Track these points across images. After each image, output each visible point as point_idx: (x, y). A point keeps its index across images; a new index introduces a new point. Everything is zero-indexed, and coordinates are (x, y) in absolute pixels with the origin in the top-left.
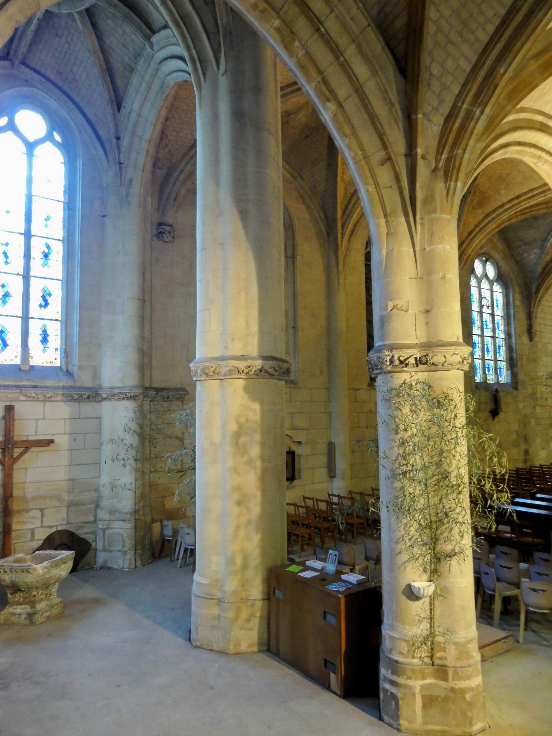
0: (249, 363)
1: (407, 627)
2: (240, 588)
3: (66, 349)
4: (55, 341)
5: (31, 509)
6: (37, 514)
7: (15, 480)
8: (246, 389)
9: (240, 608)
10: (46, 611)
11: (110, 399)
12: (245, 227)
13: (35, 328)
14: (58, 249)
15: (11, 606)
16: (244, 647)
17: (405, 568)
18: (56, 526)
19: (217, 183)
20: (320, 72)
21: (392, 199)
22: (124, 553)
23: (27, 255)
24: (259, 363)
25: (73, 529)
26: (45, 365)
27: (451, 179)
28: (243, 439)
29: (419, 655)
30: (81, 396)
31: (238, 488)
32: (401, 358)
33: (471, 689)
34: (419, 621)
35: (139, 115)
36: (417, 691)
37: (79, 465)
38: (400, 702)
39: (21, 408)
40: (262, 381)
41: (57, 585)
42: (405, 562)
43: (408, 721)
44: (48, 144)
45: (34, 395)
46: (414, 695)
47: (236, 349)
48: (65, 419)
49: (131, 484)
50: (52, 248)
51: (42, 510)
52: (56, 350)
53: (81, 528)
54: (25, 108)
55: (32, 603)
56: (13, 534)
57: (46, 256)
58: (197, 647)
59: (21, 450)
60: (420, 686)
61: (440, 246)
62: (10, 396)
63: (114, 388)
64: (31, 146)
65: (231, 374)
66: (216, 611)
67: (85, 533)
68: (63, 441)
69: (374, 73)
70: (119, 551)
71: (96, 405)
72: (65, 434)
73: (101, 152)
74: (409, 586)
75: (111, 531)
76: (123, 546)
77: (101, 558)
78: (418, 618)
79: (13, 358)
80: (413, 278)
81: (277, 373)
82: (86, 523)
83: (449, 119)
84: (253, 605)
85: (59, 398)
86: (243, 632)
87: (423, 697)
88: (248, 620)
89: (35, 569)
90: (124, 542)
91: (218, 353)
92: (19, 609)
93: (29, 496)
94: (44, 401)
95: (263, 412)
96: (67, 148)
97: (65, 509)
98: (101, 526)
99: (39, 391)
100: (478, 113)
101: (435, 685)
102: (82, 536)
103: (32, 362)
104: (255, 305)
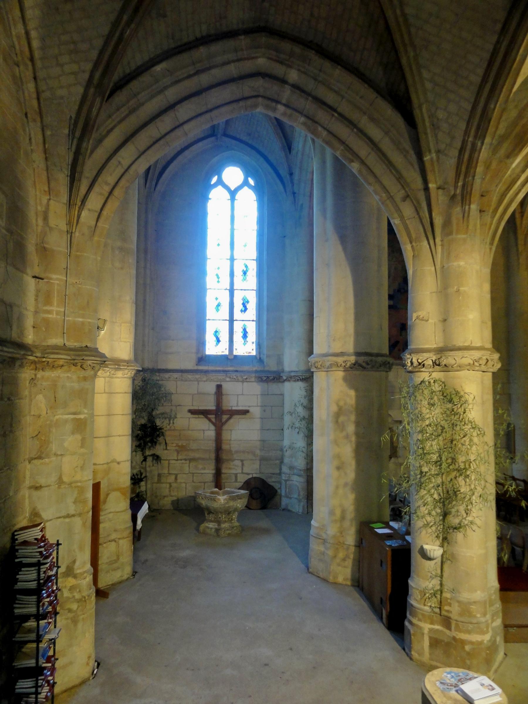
0: (345, 358)
1: (421, 580)
2: (338, 534)
3: (259, 342)
4: (252, 337)
6: (238, 463)
8: (345, 379)
9: (337, 549)
10: (228, 530)
11: (289, 381)
12: (345, 249)
13: (238, 327)
14: (253, 267)
15: (207, 522)
16: (340, 579)
17: (421, 532)
18: (252, 474)
19: (325, 218)
20: (343, 143)
21: (414, 226)
22: (300, 501)
23: (232, 274)
24: (353, 359)
26: (245, 354)
27: (465, 203)
28: (341, 419)
29: (429, 604)
30: (268, 377)
31: (338, 456)
32: (419, 361)
33: (472, 643)
34: (431, 577)
35: (303, 154)
36: (426, 631)
37: (268, 430)
38: (412, 637)
39: (227, 387)
40: (358, 373)
42: (421, 528)
43: (418, 654)
44: (246, 188)
45: (234, 377)
46: (423, 634)
47: (337, 348)
48: (257, 395)
49: (304, 447)
50: (249, 267)
51: (242, 461)
52: (253, 343)
53: (271, 477)
54: (228, 166)
55: (219, 523)
56: (223, 476)
57: (245, 273)
58: (310, 573)
59: (228, 416)
60: (429, 629)
61: (455, 264)
62: (220, 378)
63: (292, 372)
64: (233, 194)
65: (331, 368)
66: (322, 548)
68: (256, 411)
69: (387, 133)
70: (296, 498)
71: (280, 385)
72: (258, 406)
73: (281, 187)
74: (422, 547)
75: (291, 482)
76: (299, 495)
77: (284, 502)
78: (430, 574)
79: (224, 350)
80: (434, 292)
81: (369, 367)
82: (273, 474)
83: (462, 150)
84: (348, 549)
85: (253, 379)
86: (340, 568)
87: (430, 638)
88: (344, 560)
89: (219, 499)
90: (299, 493)
91: (324, 351)
92: (211, 525)
93: (233, 450)
94: (243, 382)
95: (357, 397)
96: (258, 189)
98: (284, 478)
99: (238, 374)
100: (479, 144)
101: (442, 631)
102: (270, 484)
103: (235, 353)
104: (352, 311)
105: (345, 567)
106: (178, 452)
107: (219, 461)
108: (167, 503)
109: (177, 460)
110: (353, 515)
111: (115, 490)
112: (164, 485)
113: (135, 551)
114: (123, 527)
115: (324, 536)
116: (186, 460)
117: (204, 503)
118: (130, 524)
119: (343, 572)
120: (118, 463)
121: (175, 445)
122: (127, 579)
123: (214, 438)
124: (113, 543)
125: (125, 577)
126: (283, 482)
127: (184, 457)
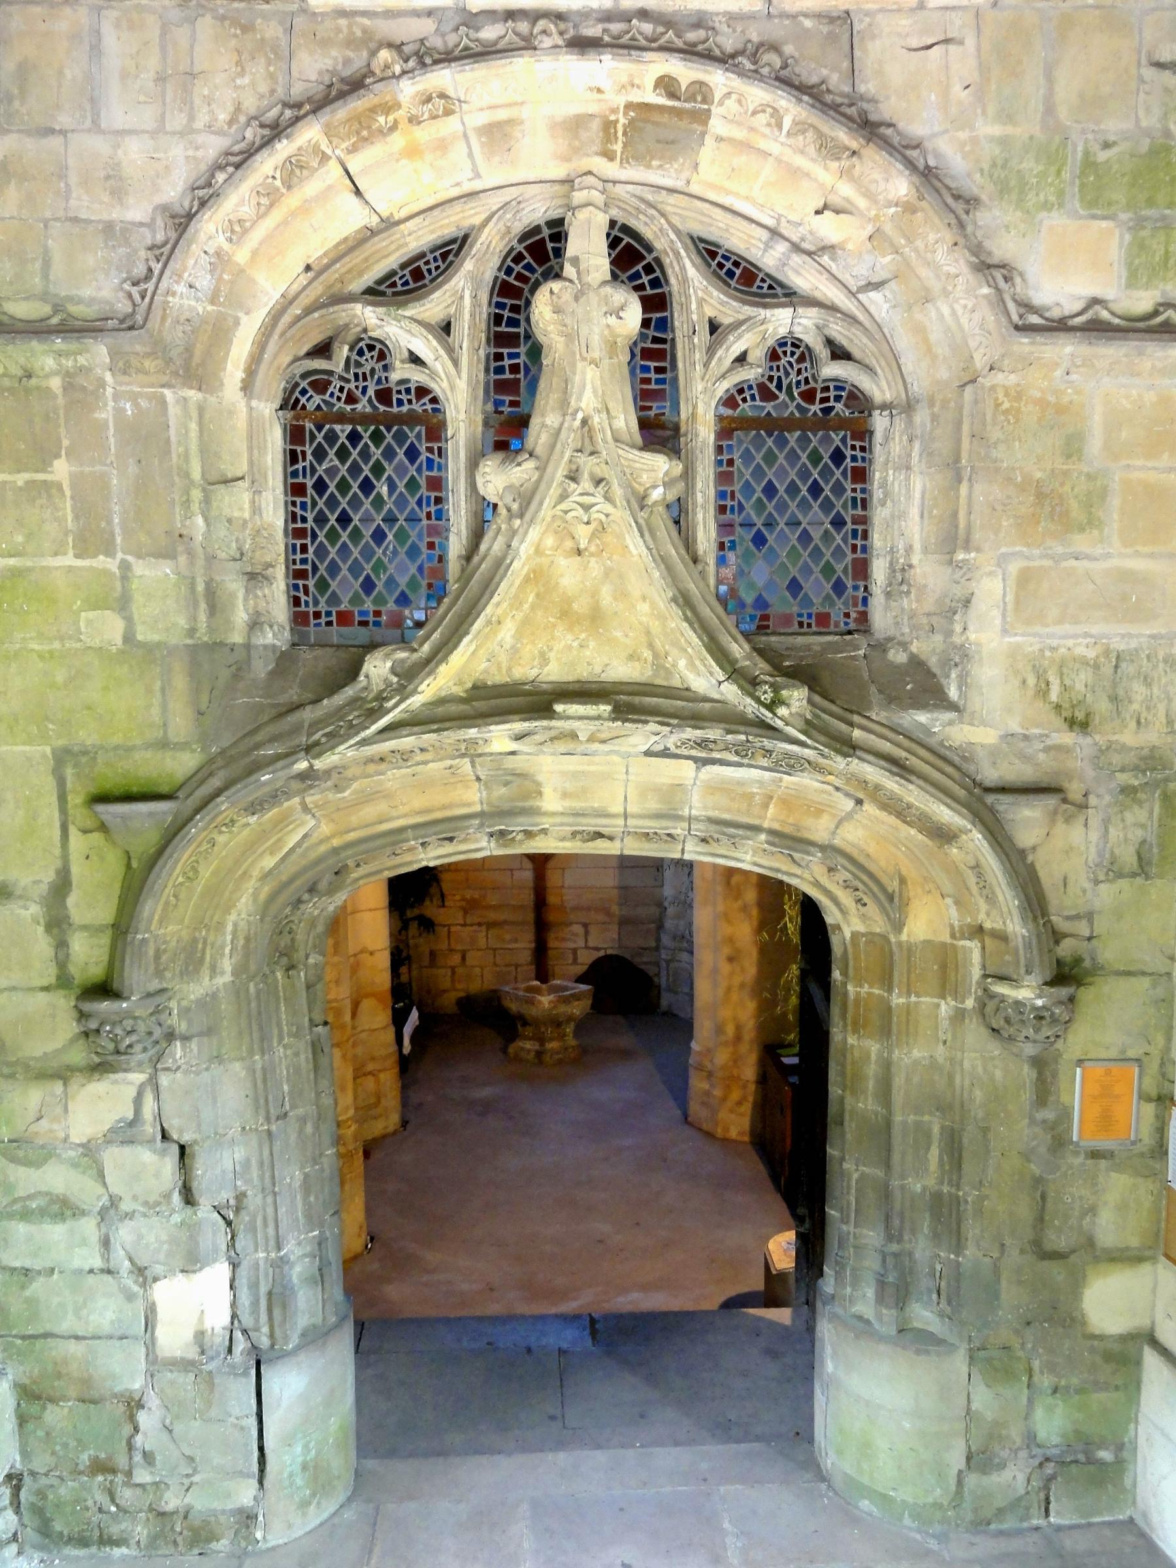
5: (571, 924)
6: (578, 929)
7: (549, 884)
16: (733, 1134)
25: (627, 956)
41: (572, 1025)
51: (585, 926)
55: (542, 1041)
67: (646, 963)
75: (676, 964)
84: (744, 1087)
86: (733, 1116)
88: (739, 1103)
89: (540, 1002)
92: (528, 1045)
97: (615, 927)
105: (742, 1115)
106: (466, 912)
107: (542, 927)
108: (448, 1002)
109: (465, 925)
110: (753, 1034)
111: (367, 996)
112: (441, 971)
113: (404, 1088)
114: (383, 1052)
115: (709, 1066)
116: (480, 924)
117: (513, 1007)
118: (395, 1048)
119: (737, 1122)
120: (371, 953)
121: (458, 897)
122: (395, 1133)
123: (531, 884)
124: (370, 1078)
125: (391, 1129)
126: (664, 964)
127: (476, 920)
